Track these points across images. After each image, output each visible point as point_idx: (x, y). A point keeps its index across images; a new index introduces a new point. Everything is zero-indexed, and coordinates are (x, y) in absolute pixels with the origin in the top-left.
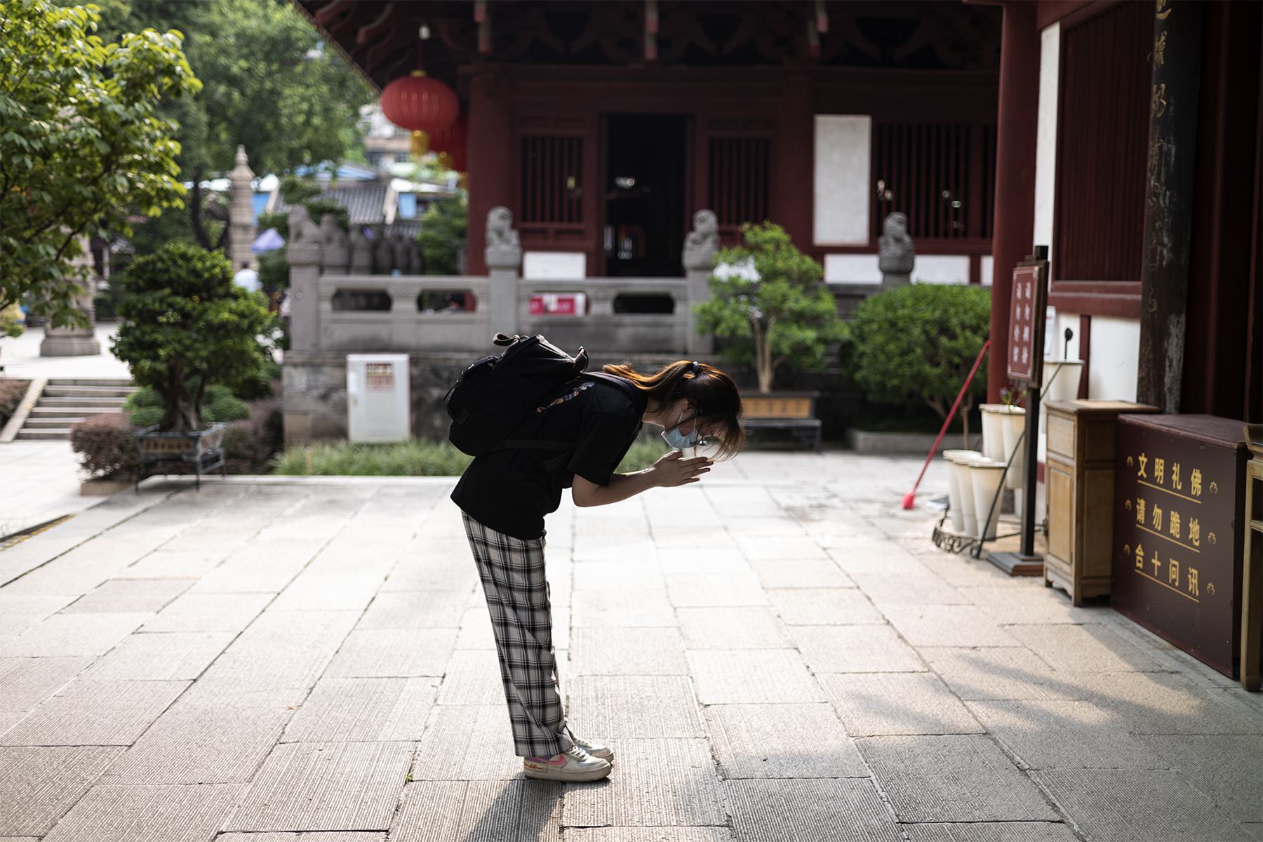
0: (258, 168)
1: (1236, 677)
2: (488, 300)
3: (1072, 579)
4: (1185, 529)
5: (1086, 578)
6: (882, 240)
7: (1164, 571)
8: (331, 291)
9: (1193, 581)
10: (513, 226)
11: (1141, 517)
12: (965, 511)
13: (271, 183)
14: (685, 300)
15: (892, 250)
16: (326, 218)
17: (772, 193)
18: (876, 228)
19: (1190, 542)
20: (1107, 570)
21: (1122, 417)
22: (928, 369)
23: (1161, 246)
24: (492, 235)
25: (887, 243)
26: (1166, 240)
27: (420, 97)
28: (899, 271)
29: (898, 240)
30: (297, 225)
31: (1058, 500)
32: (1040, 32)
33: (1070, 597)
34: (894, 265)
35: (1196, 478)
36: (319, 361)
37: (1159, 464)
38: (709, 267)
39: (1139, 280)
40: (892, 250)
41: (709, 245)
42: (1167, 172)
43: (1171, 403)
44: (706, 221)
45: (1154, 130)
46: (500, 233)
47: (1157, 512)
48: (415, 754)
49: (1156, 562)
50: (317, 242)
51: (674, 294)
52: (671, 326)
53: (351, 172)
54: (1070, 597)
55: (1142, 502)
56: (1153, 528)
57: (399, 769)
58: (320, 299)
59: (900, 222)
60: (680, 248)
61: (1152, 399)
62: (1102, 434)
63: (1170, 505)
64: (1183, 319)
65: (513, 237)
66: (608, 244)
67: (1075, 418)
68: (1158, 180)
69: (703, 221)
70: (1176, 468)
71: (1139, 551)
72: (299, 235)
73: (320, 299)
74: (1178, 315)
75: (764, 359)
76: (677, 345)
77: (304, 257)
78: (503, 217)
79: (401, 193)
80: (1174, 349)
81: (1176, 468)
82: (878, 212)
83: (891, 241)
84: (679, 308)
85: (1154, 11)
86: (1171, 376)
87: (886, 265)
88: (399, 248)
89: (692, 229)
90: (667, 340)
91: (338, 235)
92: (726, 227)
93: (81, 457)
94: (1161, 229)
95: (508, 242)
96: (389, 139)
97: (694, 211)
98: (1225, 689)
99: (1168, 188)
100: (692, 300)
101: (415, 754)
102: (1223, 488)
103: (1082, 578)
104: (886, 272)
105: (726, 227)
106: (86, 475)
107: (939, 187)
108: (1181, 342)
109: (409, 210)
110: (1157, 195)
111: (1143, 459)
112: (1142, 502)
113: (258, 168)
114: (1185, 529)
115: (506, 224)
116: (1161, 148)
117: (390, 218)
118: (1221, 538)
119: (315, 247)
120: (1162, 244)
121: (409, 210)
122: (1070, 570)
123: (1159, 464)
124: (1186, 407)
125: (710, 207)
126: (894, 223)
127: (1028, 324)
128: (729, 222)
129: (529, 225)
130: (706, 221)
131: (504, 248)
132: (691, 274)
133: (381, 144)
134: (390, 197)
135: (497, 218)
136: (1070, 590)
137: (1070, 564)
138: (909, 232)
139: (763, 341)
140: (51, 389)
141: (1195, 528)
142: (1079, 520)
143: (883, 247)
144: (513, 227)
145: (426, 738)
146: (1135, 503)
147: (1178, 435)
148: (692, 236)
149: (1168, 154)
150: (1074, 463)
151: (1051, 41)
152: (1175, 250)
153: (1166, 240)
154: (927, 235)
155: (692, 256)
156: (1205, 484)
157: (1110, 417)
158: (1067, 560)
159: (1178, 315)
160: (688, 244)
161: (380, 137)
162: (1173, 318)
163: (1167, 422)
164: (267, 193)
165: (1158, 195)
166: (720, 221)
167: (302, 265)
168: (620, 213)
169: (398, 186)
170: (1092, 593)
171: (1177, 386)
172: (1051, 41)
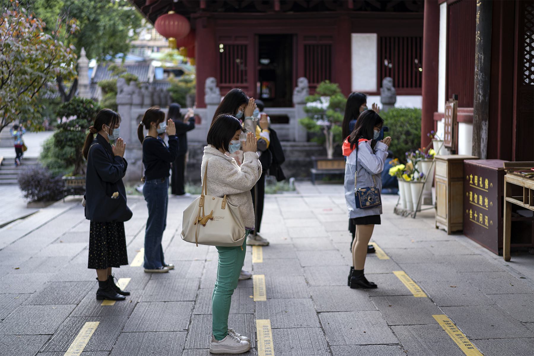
0: (89, 57)
1: (500, 254)
2: (206, 119)
3: (447, 224)
4: (484, 202)
5: (453, 223)
6: (381, 90)
7: (478, 218)
8: (136, 116)
9: (486, 221)
10: (217, 86)
11: (471, 199)
12: (407, 200)
13: (93, 63)
14: (294, 117)
15: (386, 93)
16: (132, 83)
17: (333, 67)
18: (380, 84)
19: (485, 206)
20: (461, 221)
21: (467, 161)
22: (52, 83)
23: (479, 95)
24: (207, 90)
25: (384, 91)
26: (481, 92)
27: (169, 23)
28: (390, 103)
29: (389, 89)
30: (121, 87)
31: (441, 194)
32: (440, 5)
33: (446, 232)
34: (387, 101)
35: (487, 181)
36: (131, 147)
37: (476, 177)
38: (304, 103)
39: (472, 107)
40: (386, 93)
41: (305, 92)
42: (481, 66)
43: (484, 154)
44: (303, 82)
45: (477, 49)
46: (211, 89)
47: (476, 196)
48: (200, 282)
49: (476, 215)
50: (129, 94)
51: (289, 115)
52: (288, 129)
53: (132, 58)
54: (446, 232)
55: (471, 193)
56: (474, 202)
57: (196, 284)
58: (131, 119)
59: (390, 82)
60: (291, 95)
61: (476, 154)
62: (459, 170)
63: (479, 193)
64: (487, 123)
65: (217, 91)
66: (258, 90)
67: (447, 162)
68: (478, 69)
69: (302, 82)
70: (481, 179)
71: (471, 212)
72: (122, 91)
73: (131, 119)
74: (486, 121)
75: (329, 143)
76: (291, 138)
77: (124, 101)
78: (212, 82)
79: (156, 68)
80: (484, 135)
81: (481, 179)
82: (382, 73)
83: (386, 90)
84: (292, 121)
85: (476, 3)
86: (483, 145)
87: (384, 101)
88: (162, 95)
89: (297, 86)
90: (287, 135)
91: (137, 91)
92: (312, 85)
93: (25, 193)
94: (479, 88)
95: (215, 93)
96: (149, 41)
97: (297, 78)
98: (496, 259)
99: (481, 72)
100: (297, 118)
101: (200, 282)
102: (495, 186)
103: (451, 224)
104: (384, 104)
105: (312, 85)
106: (29, 200)
107: (403, 67)
108: (487, 132)
109: (160, 76)
110: (477, 75)
111: (471, 176)
112: (471, 193)
113: (89, 57)
114: (484, 202)
115: (214, 85)
116: (478, 56)
117: (151, 80)
118: (495, 204)
119: (129, 96)
120: (479, 94)
121: (160, 76)
122: (446, 221)
123: (476, 177)
124: (489, 157)
125: (305, 76)
126: (387, 82)
127: (450, 125)
128: (314, 82)
129: (224, 85)
130: (303, 82)
131: (213, 95)
132: (297, 106)
133: (145, 43)
134: (151, 70)
135: (210, 82)
136: (446, 228)
137: (446, 219)
138: (394, 86)
139: (329, 134)
140: (5, 162)
141: (486, 200)
142: (449, 201)
143: (382, 93)
144: (217, 86)
145: (203, 278)
146: (469, 194)
147: (481, 167)
148: (297, 89)
149: (481, 59)
150: (446, 180)
151: (443, 8)
152: (484, 96)
153: (481, 92)
154: (403, 86)
155: (297, 98)
156: (489, 184)
157: (461, 161)
158: (445, 217)
159: (486, 121)
160: (295, 92)
161: (144, 40)
162: (483, 122)
163: (483, 163)
164: (91, 69)
165: (478, 76)
166: (309, 82)
167: (123, 104)
168: (265, 75)
169: (155, 64)
170: (455, 229)
171: (485, 150)
172: (443, 8)
